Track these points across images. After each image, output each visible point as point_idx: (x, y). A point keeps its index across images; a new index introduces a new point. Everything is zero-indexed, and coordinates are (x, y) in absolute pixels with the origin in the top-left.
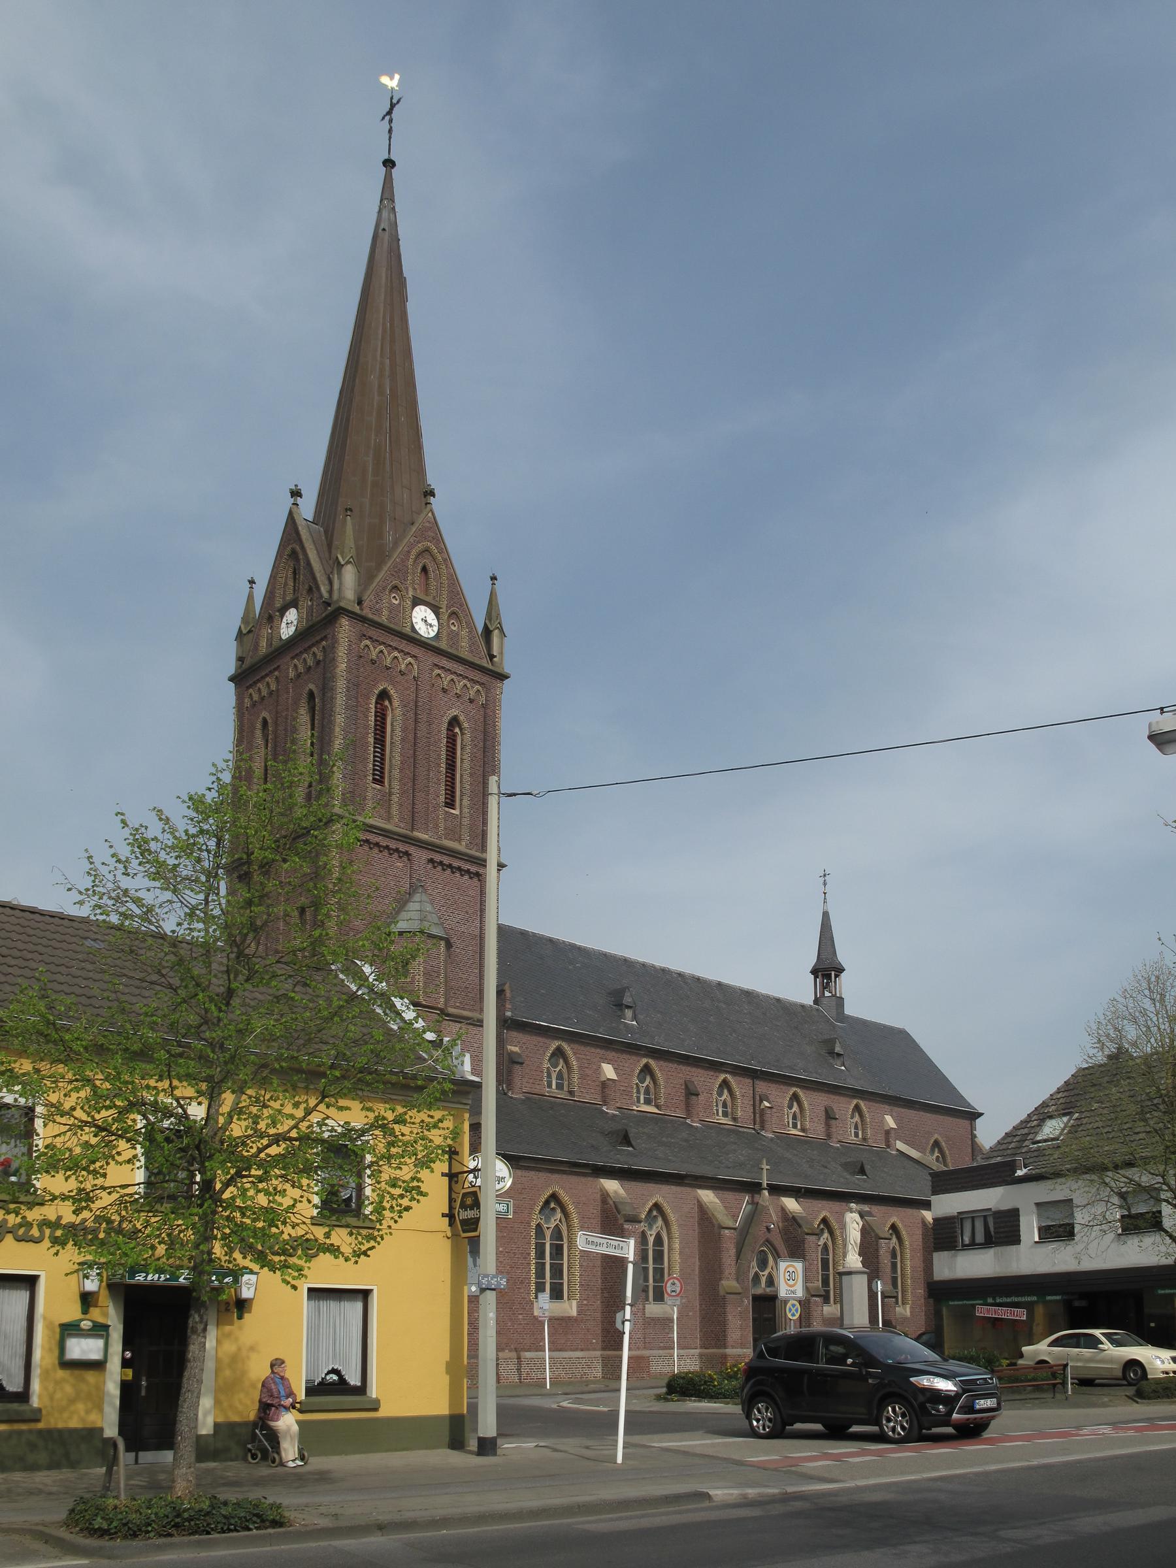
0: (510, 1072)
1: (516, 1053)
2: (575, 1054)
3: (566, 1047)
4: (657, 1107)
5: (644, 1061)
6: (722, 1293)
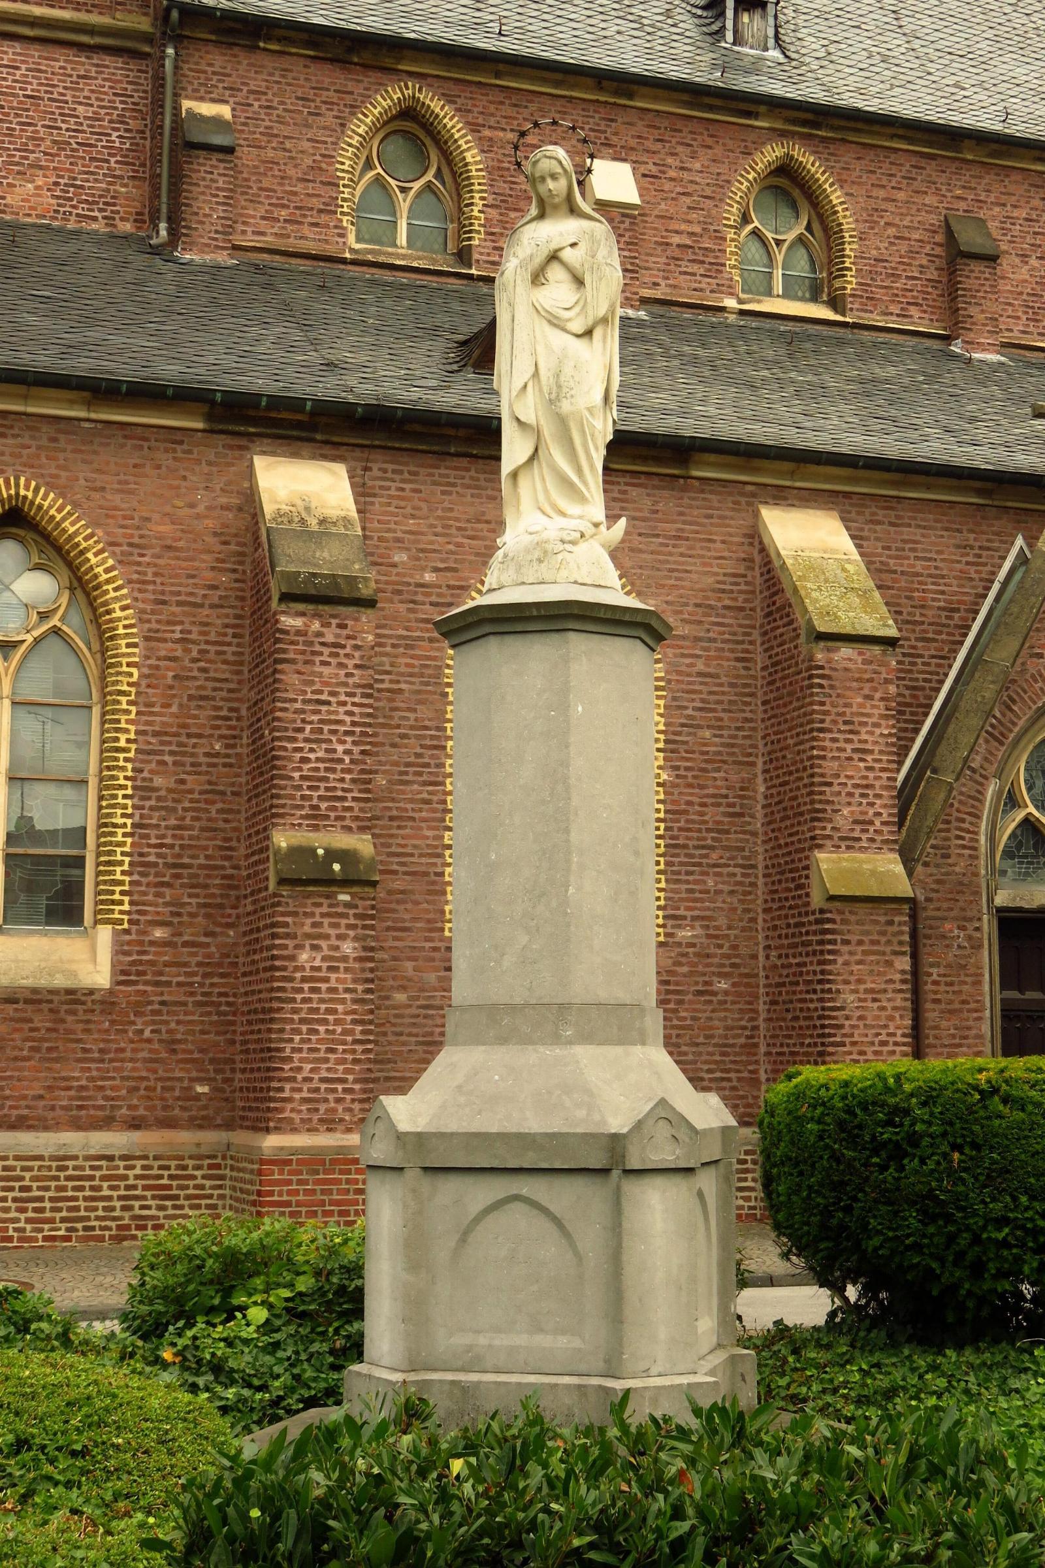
0: (177, 178)
1: (217, 121)
2: (474, 127)
3: (809, 161)
4: (835, 303)
5: (772, 153)
6: (817, 900)
